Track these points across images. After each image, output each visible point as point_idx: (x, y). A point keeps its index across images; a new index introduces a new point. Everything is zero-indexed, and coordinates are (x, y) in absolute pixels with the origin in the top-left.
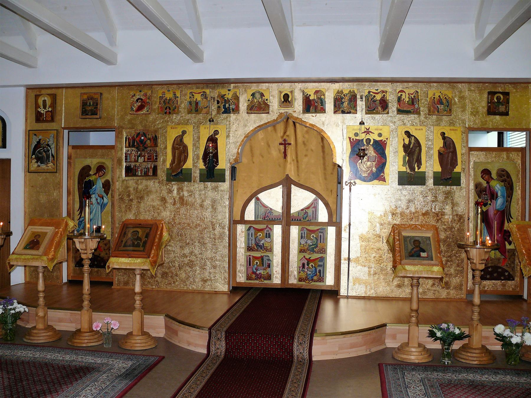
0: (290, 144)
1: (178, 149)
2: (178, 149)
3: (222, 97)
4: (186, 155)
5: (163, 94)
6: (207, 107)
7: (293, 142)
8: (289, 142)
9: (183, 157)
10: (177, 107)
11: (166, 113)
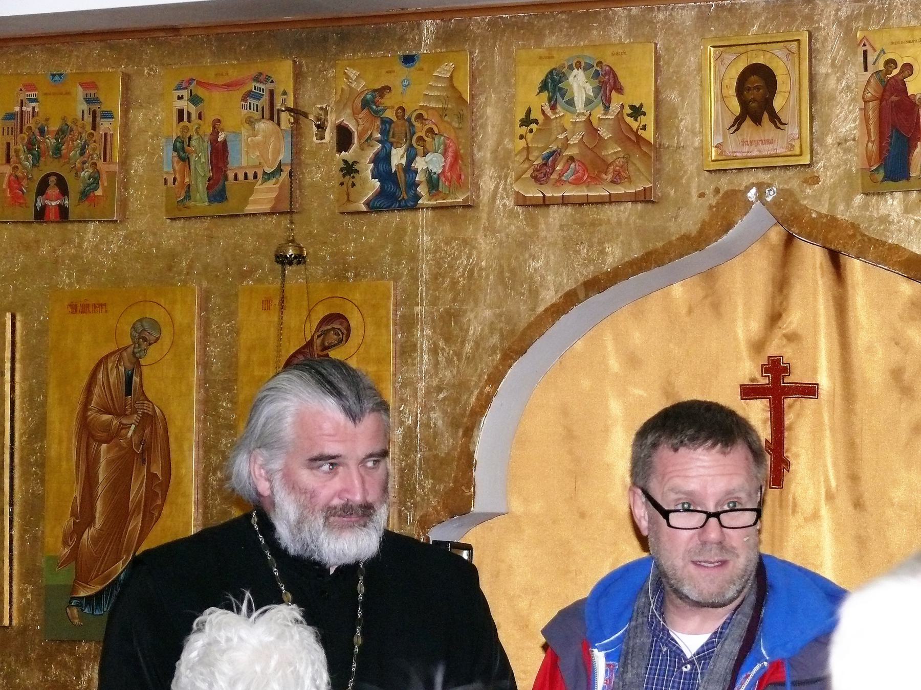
0: (810, 391)
1: (111, 436)
2: (111, 436)
3: (366, 104)
4: (157, 470)
5: (23, 96)
6: (279, 170)
7: (824, 381)
8: (797, 377)
9: (137, 489)
10: (104, 177)
11: (40, 215)
